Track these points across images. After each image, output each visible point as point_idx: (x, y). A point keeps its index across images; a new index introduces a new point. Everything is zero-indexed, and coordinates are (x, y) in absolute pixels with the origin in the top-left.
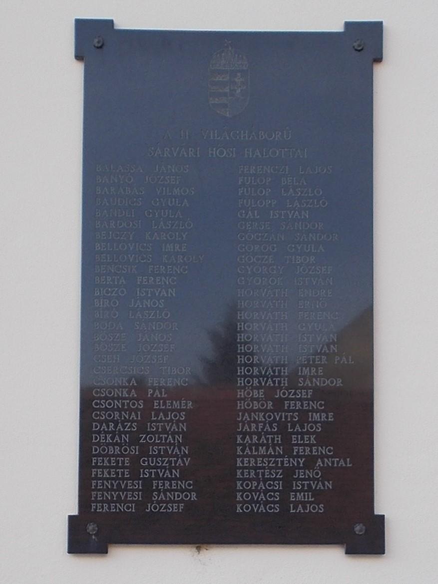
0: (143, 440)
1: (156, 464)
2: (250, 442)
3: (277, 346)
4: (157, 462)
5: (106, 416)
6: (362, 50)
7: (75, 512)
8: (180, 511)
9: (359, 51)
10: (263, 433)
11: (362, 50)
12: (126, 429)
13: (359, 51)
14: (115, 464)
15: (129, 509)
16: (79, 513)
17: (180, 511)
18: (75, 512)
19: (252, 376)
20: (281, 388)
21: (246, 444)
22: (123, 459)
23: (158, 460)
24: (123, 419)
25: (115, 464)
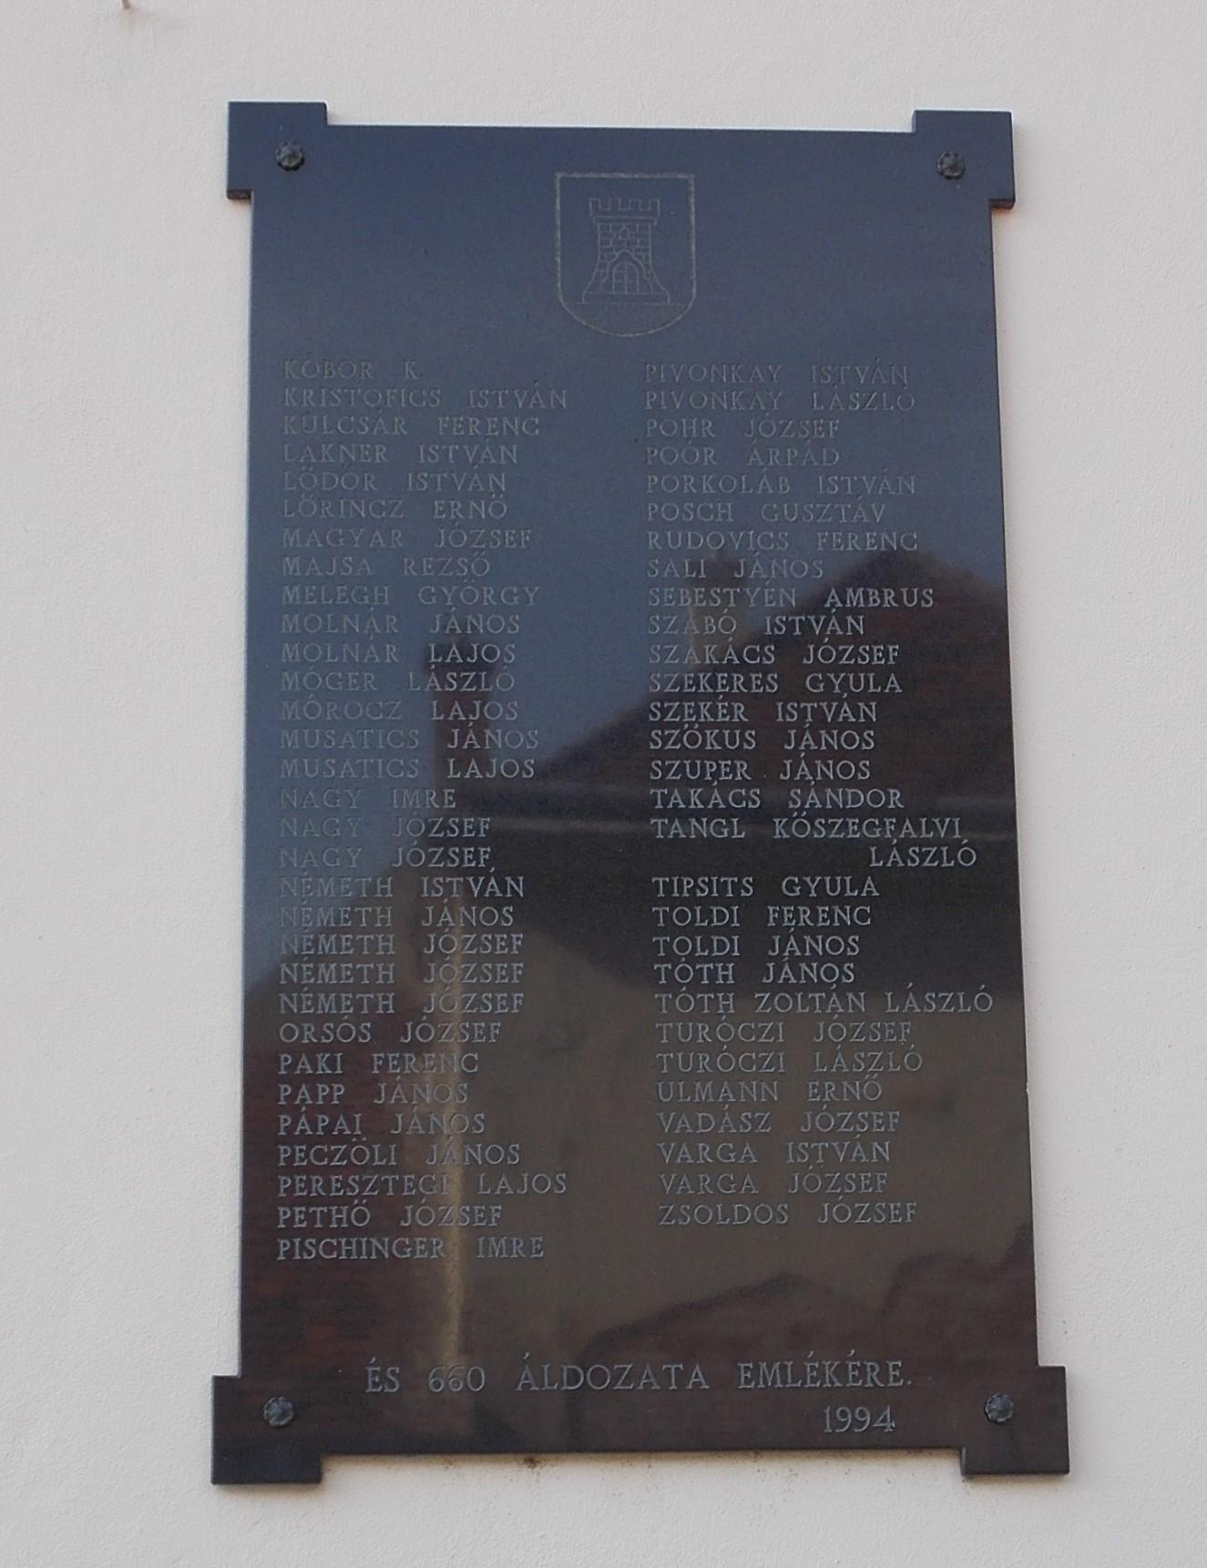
0: (674, 744)
1: (919, 603)
2: (310, 1102)
3: (797, 619)
4: (921, 597)
5: (338, 1035)
6: (303, 161)
7: (231, 1368)
8: (891, 662)
9: (296, 168)
10: (304, 1109)
11: (303, 161)
12: (841, 821)
13: (296, 168)
14: (304, 1225)
15: (741, 803)
16: (915, 130)
17: (891, 662)
18: (231, 1368)
19: (682, 754)
20: (818, 642)
21: (299, 1107)
22: (325, 1209)
23: (924, 592)
24: (819, 778)
25: (304, 1225)
